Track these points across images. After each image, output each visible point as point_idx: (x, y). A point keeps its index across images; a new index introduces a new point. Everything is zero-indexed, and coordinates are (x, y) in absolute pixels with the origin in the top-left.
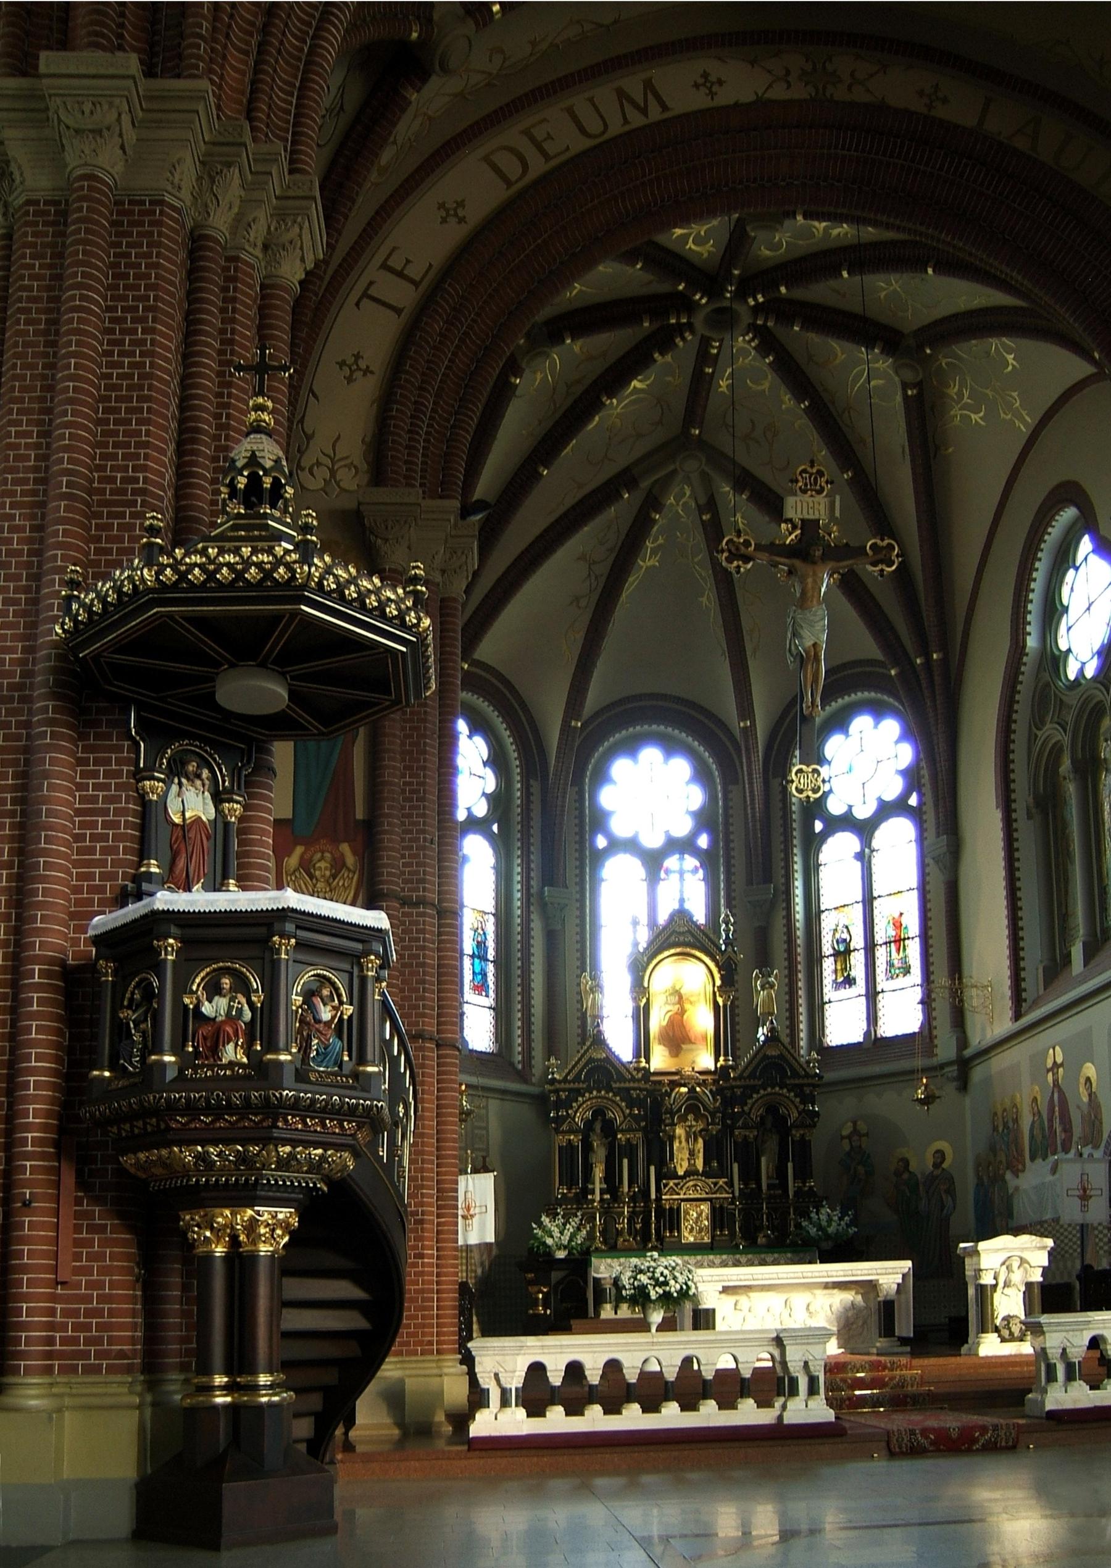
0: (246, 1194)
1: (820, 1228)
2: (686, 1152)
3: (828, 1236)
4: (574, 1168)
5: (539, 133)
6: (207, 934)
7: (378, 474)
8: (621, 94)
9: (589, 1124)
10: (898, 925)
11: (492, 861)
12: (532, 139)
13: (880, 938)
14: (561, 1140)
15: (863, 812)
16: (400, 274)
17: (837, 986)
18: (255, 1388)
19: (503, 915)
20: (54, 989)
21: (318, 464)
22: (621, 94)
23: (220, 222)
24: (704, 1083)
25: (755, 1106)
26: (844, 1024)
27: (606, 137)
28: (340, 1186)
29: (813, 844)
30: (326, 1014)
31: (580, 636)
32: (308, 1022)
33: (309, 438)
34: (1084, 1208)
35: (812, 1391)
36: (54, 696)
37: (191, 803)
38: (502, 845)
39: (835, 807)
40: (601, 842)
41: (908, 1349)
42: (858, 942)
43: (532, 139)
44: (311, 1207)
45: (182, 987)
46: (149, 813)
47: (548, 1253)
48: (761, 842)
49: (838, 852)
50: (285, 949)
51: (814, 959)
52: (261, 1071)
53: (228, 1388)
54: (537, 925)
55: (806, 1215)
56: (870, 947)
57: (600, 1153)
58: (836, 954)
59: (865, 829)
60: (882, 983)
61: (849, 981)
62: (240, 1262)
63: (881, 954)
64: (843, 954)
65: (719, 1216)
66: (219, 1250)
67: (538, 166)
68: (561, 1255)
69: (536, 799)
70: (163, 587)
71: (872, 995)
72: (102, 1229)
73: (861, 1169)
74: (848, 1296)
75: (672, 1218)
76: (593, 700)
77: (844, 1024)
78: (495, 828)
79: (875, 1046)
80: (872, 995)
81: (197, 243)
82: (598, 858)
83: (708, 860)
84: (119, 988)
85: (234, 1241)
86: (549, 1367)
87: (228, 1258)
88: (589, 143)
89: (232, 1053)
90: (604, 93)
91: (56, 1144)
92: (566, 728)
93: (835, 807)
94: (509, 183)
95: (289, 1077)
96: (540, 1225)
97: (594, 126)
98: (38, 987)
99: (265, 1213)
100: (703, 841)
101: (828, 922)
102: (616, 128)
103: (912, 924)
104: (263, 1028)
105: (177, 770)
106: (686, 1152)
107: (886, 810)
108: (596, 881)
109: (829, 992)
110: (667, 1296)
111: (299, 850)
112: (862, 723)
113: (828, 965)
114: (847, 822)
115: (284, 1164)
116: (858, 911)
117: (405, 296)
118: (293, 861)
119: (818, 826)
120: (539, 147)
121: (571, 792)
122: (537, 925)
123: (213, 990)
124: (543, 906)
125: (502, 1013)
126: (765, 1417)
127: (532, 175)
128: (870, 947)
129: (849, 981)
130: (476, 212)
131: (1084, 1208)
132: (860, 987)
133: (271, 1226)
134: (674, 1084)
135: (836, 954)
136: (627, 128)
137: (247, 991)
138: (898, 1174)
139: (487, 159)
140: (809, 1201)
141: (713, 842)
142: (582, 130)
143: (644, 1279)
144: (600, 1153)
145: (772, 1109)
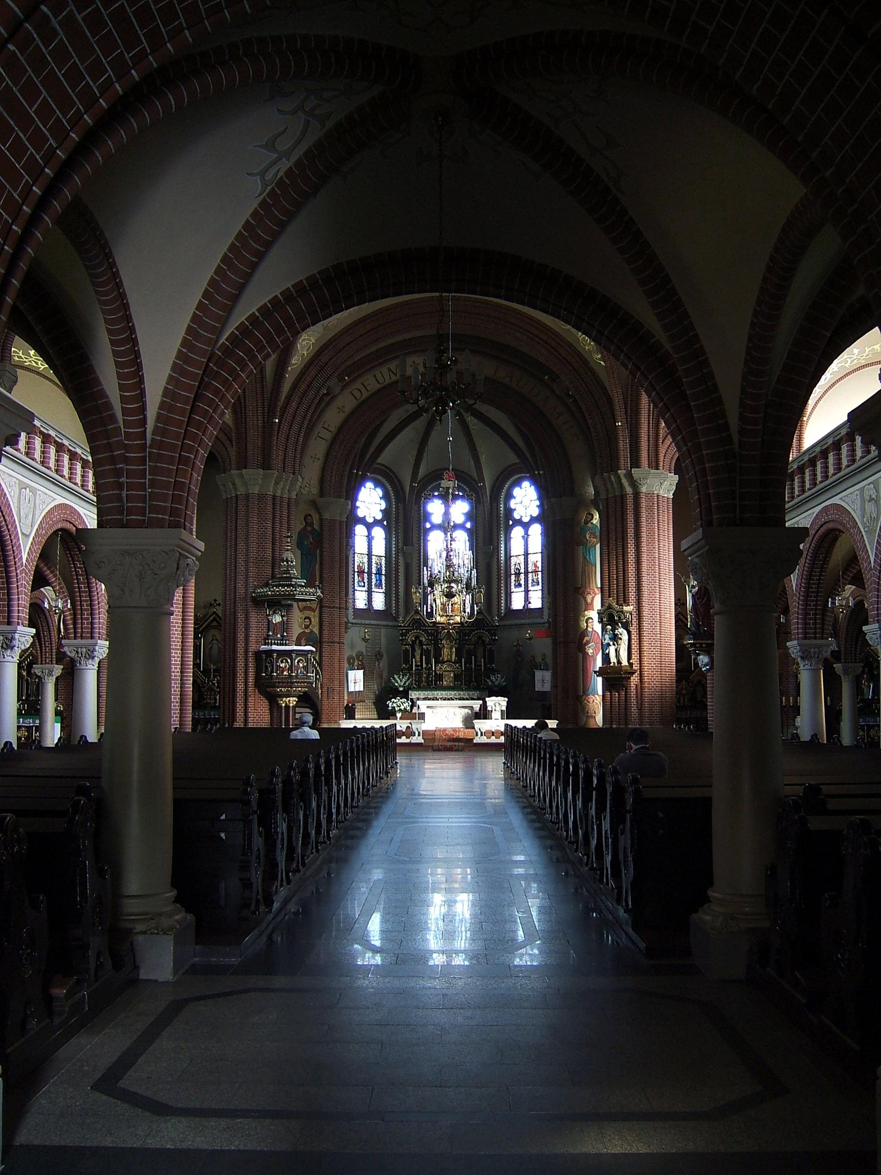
0: (288, 696)
1: (493, 682)
2: (448, 652)
3: (495, 686)
4: (407, 657)
7: (322, 494)
8: (390, 370)
9: (414, 642)
10: (536, 566)
11: (384, 536)
13: (530, 570)
14: (404, 647)
15: (526, 519)
17: (516, 586)
19: (388, 556)
22: (390, 370)
23: (279, 494)
24: (454, 628)
25: (473, 638)
26: (517, 603)
28: (305, 693)
29: (508, 529)
30: (301, 665)
31: (415, 453)
32: (298, 667)
34: (543, 686)
35: (419, 735)
37: (277, 619)
38: (388, 530)
39: (516, 516)
40: (428, 525)
41: (189, 728)
42: (522, 571)
44: (299, 697)
46: (269, 622)
47: (397, 689)
48: (489, 530)
49: (517, 533)
51: (508, 575)
52: (290, 676)
54: (401, 561)
55: (489, 678)
56: (526, 573)
57: (418, 653)
58: (516, 574)
59: (526, 526)
60: (530, 588)
61: (520, 585)
62: (287, 707)
63: (530, 575)
64: (518, 574)
65: (457, 677)
67: (366, 394)
68: (401, 689)
69: (401, 511)
71: (527, 591)
73: (520, 659)
74: (467, 711)
75: (440, 677)
76: (422, 472)
77: (517, 603)
78: (385, 523)
79: (527, 611)
80: (527, 591)
81: (274, 497)
82: (427, 531)
83: (470, 532)
84: (266, 659)
89: (285, 673)
92: (411, 485)
93: (516, 516)
96: (394, 679)
97: (381, 380)
99: (291, 699)
100: (468, 525)
101: (513, 561)
102: (388, 381)
103: (539, 564)
104: (291, 669)
105: (274, 613)
106: (448, 652)
107: (533, 520)
108: (426, 541)
109: (513, 589)
110: (400, 710)
112: (516, 491)
113: (513, 577)
114: (519, 522)
116: (522, 558)
117: (328, 436)
119: (511, 523)
121: (415, 507)
122: (401, 561)
123: (282, 662)
124: (404, 555)
125: (387, 595)
126: (408, 741)
127: (364, 397)
128: (526, 573)
129: (520, 585)
130: (348, 409)
131: (543, 686)
132: (522, 589)
133: (293, 701)
134: (443, 628)
135: (516, 574)
138: (531, 661)
140: (490, 671)
141: (472, 526)
143: (395, 705)
144: (418, 653)
145: (480, 638)
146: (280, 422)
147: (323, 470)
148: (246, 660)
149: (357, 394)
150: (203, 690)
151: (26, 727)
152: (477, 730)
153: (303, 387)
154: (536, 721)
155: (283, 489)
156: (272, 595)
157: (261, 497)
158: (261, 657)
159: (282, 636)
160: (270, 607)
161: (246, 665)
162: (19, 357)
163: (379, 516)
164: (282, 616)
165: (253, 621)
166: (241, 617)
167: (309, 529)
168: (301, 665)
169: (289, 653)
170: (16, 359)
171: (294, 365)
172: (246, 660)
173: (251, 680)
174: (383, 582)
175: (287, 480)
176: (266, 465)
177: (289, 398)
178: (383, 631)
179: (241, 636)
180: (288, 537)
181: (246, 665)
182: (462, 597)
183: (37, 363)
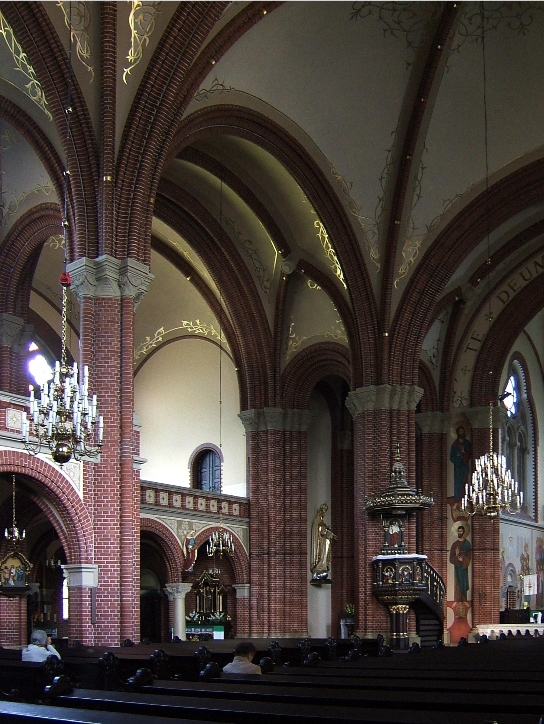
5: (512, 284)
6: (386, 562)
7: (472, 404)
12: (510, 286)
16: (476, 339)
18: (400, 635)
20: (371, 567)
21: (458, 400)
22: (536, 263)
27: (532, 279)
30: (406, 573)
33: (455, 393)
36: (368, 515)
43: (510, 286)
45: (383, 571)
46: (386, 533)
50: (397, 564)
52: (394, 585)
53: (393, 635)
66: (394, 612)
67: (512, 294)
70: (374, 506)
72: (380, 608)
81: (391, 411)
85: (396, 611)
86: (512, 631)
87: (396, 613)
88: (527, 282)
89: (390, 581)
90: (531, 265)
91: (372, 594)
94: (504, 302)
95: (397, 586)
97: (527, 276)
98: (368, 567)
102: (535, 275)
105: (391, 524)
111: (456, 504)
115: (401, 598)
117: (477, 345)
118: (455, 507)
120: (512, 288)
136: (538, 274)
137: (392, 571)
139: (498, 297)
142: (525, 280)
146: (391, 336)
147: (473, 380)
149: (504, 296)
151: (199, 635)
153: (415, 296)
154: (506, 635)
155: (400, 402)
156: (375, 507)
157: (377, 413)
158: (378, 566)
159: (400, 546)
160: (386, 518)
162: (191, 328)
167: (461, 441)
168: (406, 573)
170: (190, 330)
171: (402, 275)
175: (402, 393)
176: (378, 381)
177: (400, 310)
180: (398, 448)
182: (100, 460)
183: (202, 330)
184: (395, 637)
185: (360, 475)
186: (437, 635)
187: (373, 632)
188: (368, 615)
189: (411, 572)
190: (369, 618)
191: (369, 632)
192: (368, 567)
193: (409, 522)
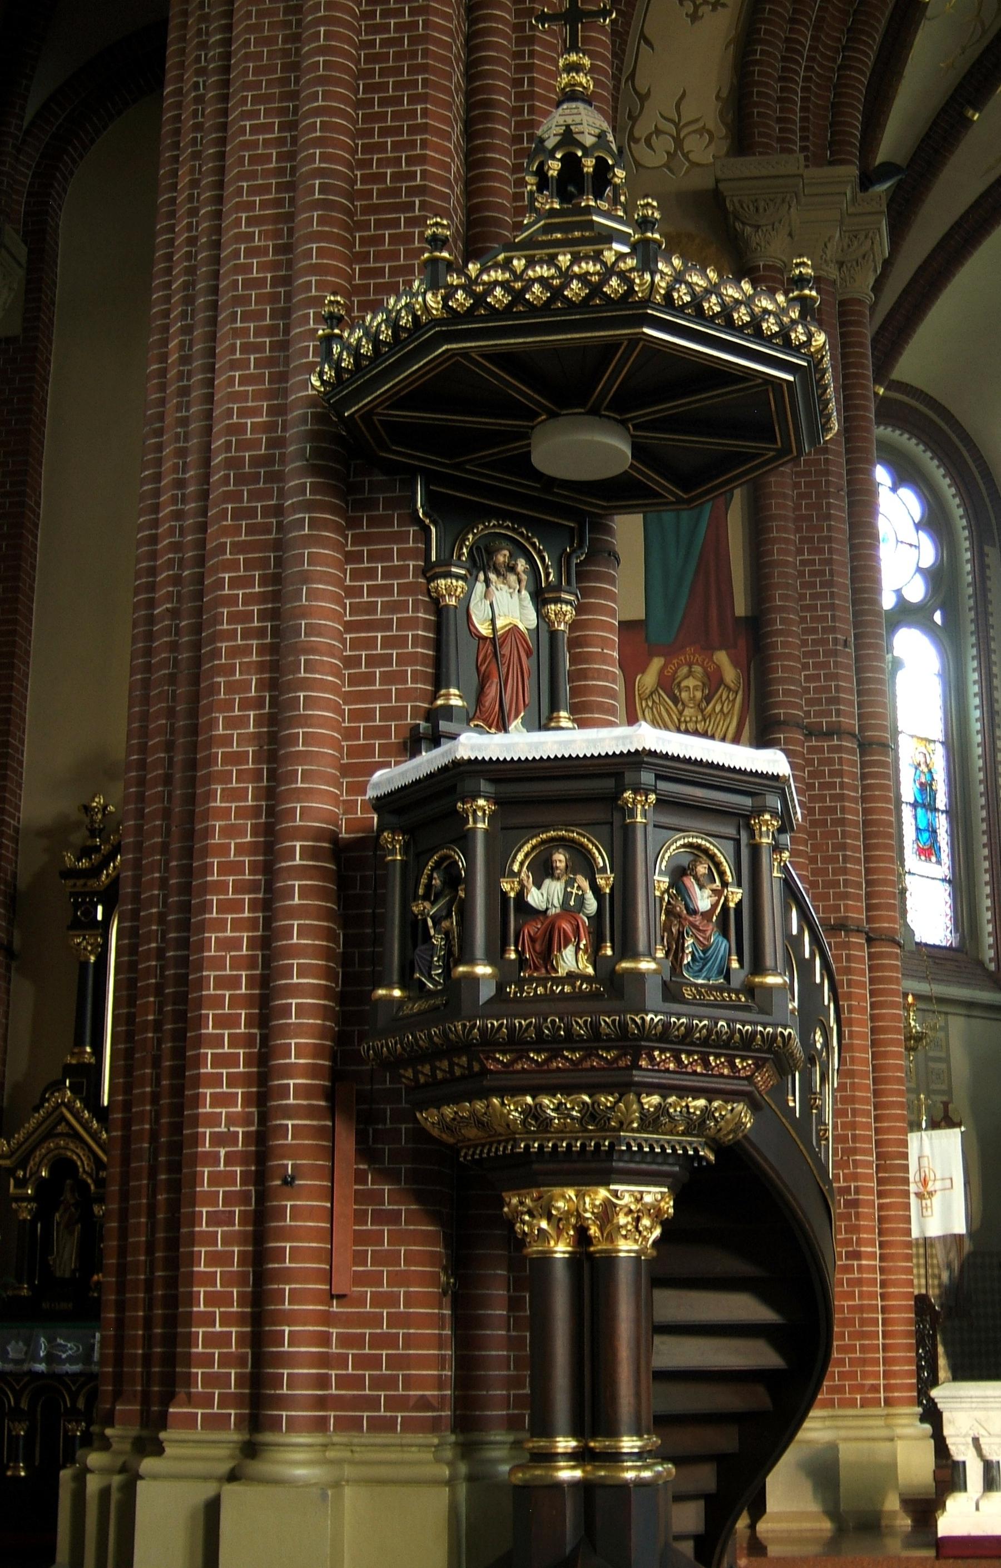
0: (595, 1167)
6: (535, 792)
18: (615, 1457)
21: (658, 132)
30: (703, 900)
32: (678, 913)
33: (643, 98)
36: (314, 470)
37: (504, 606)
50: (642, 809)
53: (578, 1457)
62: (591, 1267)
66: (561, 1249)
72: (393, 1218)
78: (938, 617)
84: (411, 871)
85: (582, 1236)
89: (571, 960)
91: (329, 1095)
98: (302, 872)
99: (626, 1194)
104: (614, 924)
105: (482, 562)
111: (657, 663)
115: (651, 1121)
118: (649, 679)
123: (543, 870)
125: (962, 887)
133: (634, 1215)
137: (591, 872)
148: (269, 904)
150: (98, 1210)
152: (960, 1450)
161: (268, 945)
163: (916, 592)
164: (540, 597)
165: (324, 605)
166: (237, 593)
169: (594, 789)
172: (269, 904)
173: (300, 1049)
174: (943, 839)
178: (957, 1025)
179: (234, 732)
181: (268, 945)
184: (568, 1474)
185: (250, 206)
186: (720, 1459)
187: (320, 1425)
188: (287, 1276)
189: (736, 895)
190: (298, 1300)
191: (293, 1425)
192: (302, 872)
193: (586, 592)
